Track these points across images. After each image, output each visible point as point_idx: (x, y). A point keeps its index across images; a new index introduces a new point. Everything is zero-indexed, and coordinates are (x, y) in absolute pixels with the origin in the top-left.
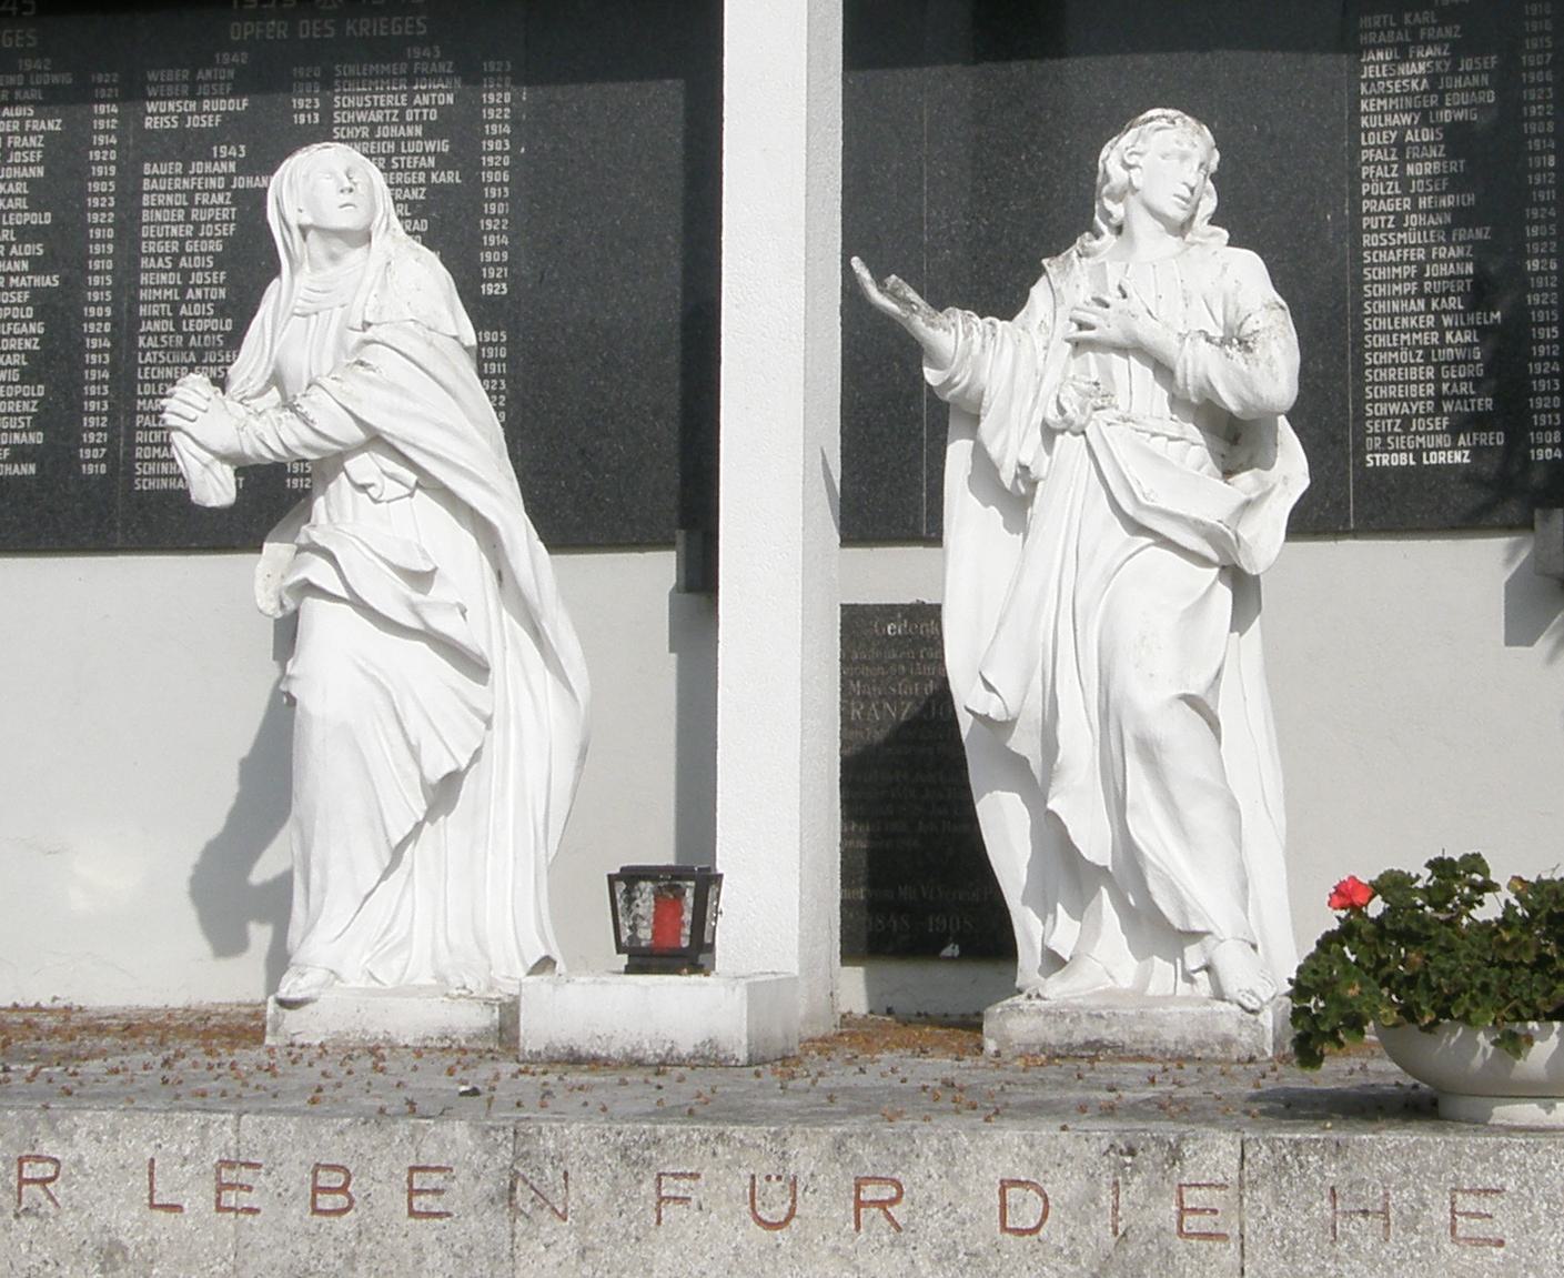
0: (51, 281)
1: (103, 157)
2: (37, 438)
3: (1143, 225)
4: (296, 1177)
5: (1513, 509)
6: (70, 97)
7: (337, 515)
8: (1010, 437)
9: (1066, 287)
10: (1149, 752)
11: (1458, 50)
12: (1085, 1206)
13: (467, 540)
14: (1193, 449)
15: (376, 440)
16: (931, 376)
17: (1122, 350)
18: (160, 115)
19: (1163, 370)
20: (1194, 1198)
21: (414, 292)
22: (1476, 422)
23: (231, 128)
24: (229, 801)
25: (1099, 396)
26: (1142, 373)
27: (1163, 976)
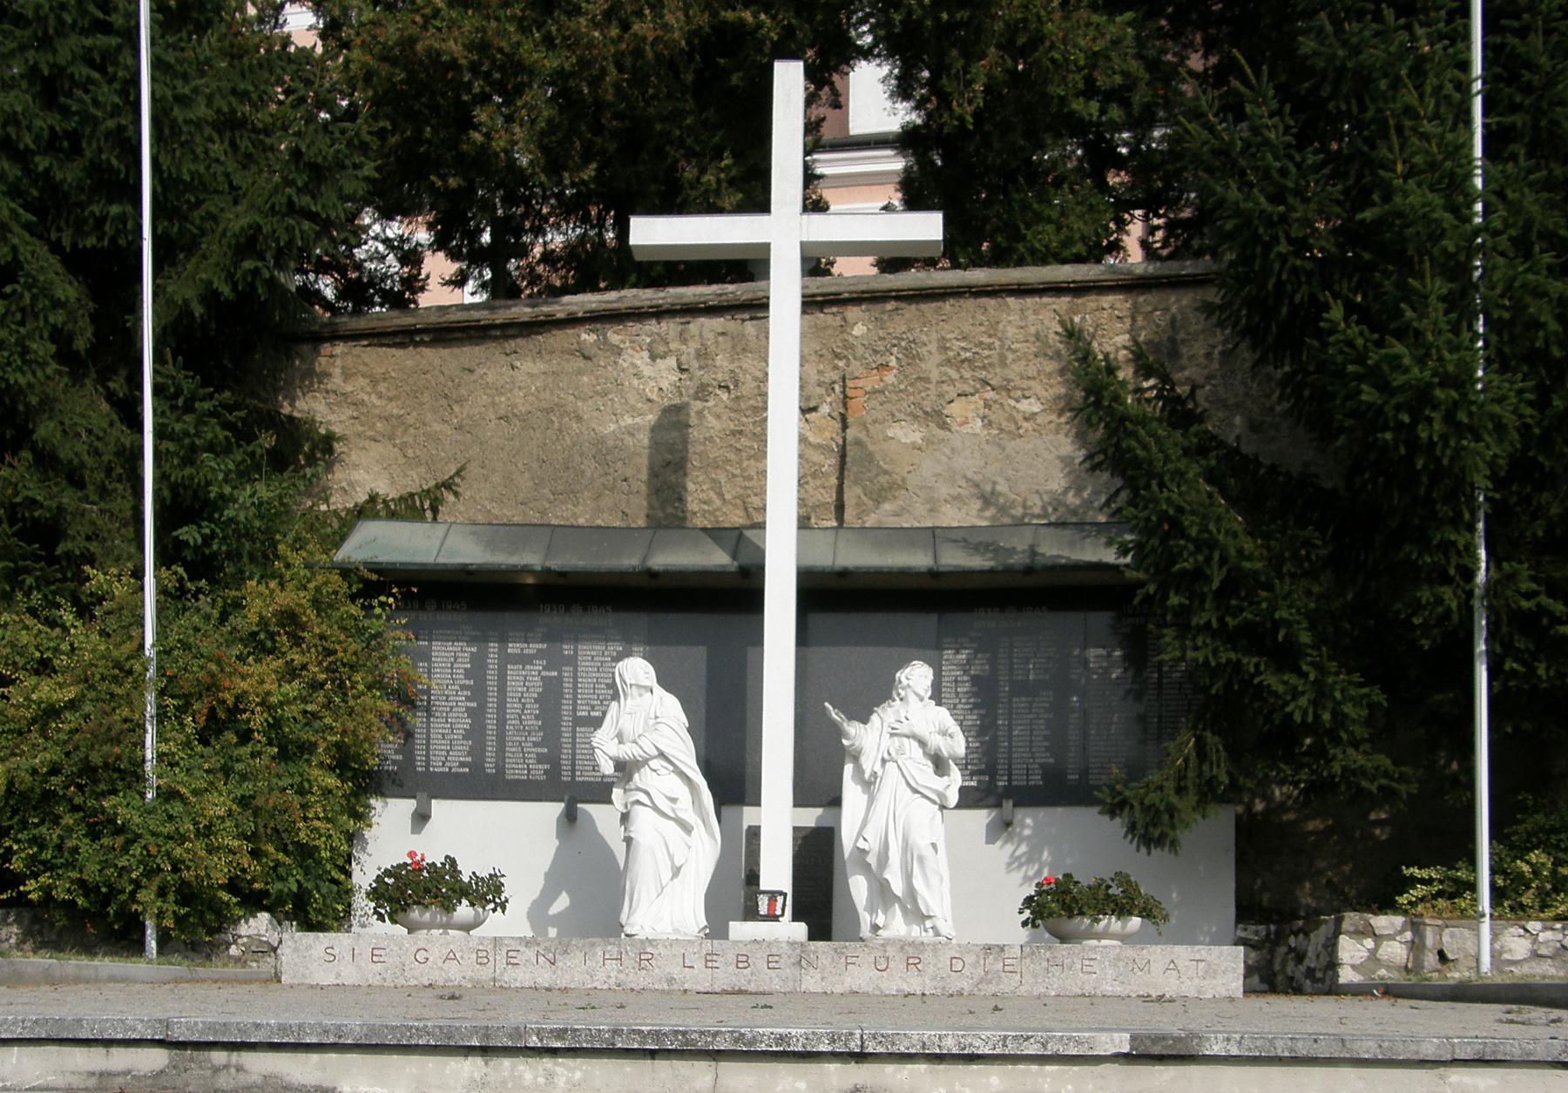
0: (474, 705)
1: (493, 661)
2: (469, 759)
3: (912, 698)
4: (731, 957)
5: (992, 800)
6: (480, 639)
7: (641, 778)
8: (869, 763)
9: (885, 716)
10: (921, 860)
11: (976, 651)
12: (975, 965)
13: (686, 789)
14: (929, 767)
15: (662, 755)
16: (845, 742)
17: (907, 737)
18: (513, 648)
19: (922, 743)
20: (1008, 962)
21: (670, 708)
22: (980, 772)
23: (540, 654)
24: (541, 887)
25: (901, 751)
26: (915, 744)
27: (916, 931)
